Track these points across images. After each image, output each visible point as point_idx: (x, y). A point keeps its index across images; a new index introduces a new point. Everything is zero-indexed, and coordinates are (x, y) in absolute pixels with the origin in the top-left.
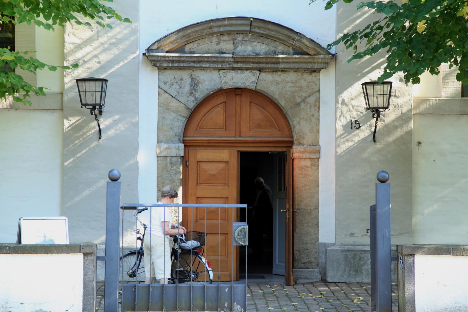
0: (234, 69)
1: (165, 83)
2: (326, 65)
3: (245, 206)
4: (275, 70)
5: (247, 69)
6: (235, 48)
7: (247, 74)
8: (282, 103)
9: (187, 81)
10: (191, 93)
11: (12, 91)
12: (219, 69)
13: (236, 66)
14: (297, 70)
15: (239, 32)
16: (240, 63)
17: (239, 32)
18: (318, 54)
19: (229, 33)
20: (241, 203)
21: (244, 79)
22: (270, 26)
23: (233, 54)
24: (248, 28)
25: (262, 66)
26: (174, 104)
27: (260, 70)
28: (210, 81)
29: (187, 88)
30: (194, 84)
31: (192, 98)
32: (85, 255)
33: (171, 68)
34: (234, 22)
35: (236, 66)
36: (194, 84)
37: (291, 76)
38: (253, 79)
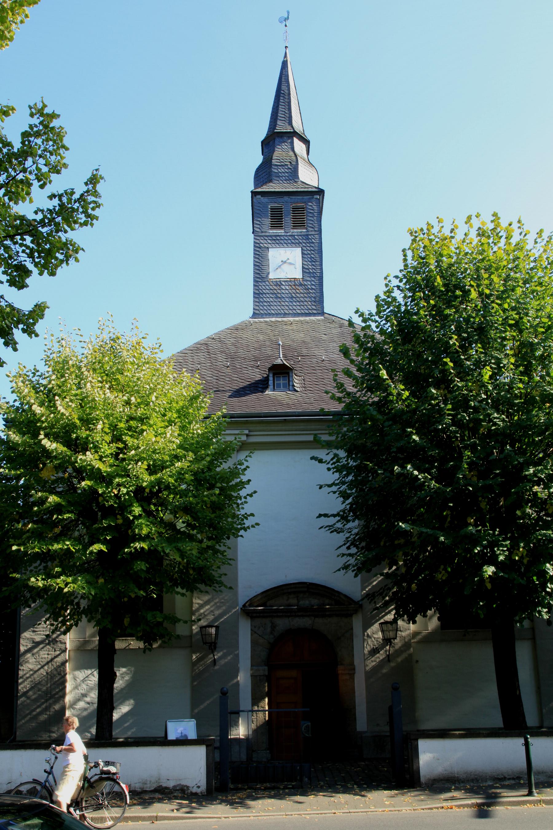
1: (255, 627)
2: (356, 612)
16: (304, 612)
28: (282, 624)
29: (269, 630)
30: (273, 627)
36: (273, 627)
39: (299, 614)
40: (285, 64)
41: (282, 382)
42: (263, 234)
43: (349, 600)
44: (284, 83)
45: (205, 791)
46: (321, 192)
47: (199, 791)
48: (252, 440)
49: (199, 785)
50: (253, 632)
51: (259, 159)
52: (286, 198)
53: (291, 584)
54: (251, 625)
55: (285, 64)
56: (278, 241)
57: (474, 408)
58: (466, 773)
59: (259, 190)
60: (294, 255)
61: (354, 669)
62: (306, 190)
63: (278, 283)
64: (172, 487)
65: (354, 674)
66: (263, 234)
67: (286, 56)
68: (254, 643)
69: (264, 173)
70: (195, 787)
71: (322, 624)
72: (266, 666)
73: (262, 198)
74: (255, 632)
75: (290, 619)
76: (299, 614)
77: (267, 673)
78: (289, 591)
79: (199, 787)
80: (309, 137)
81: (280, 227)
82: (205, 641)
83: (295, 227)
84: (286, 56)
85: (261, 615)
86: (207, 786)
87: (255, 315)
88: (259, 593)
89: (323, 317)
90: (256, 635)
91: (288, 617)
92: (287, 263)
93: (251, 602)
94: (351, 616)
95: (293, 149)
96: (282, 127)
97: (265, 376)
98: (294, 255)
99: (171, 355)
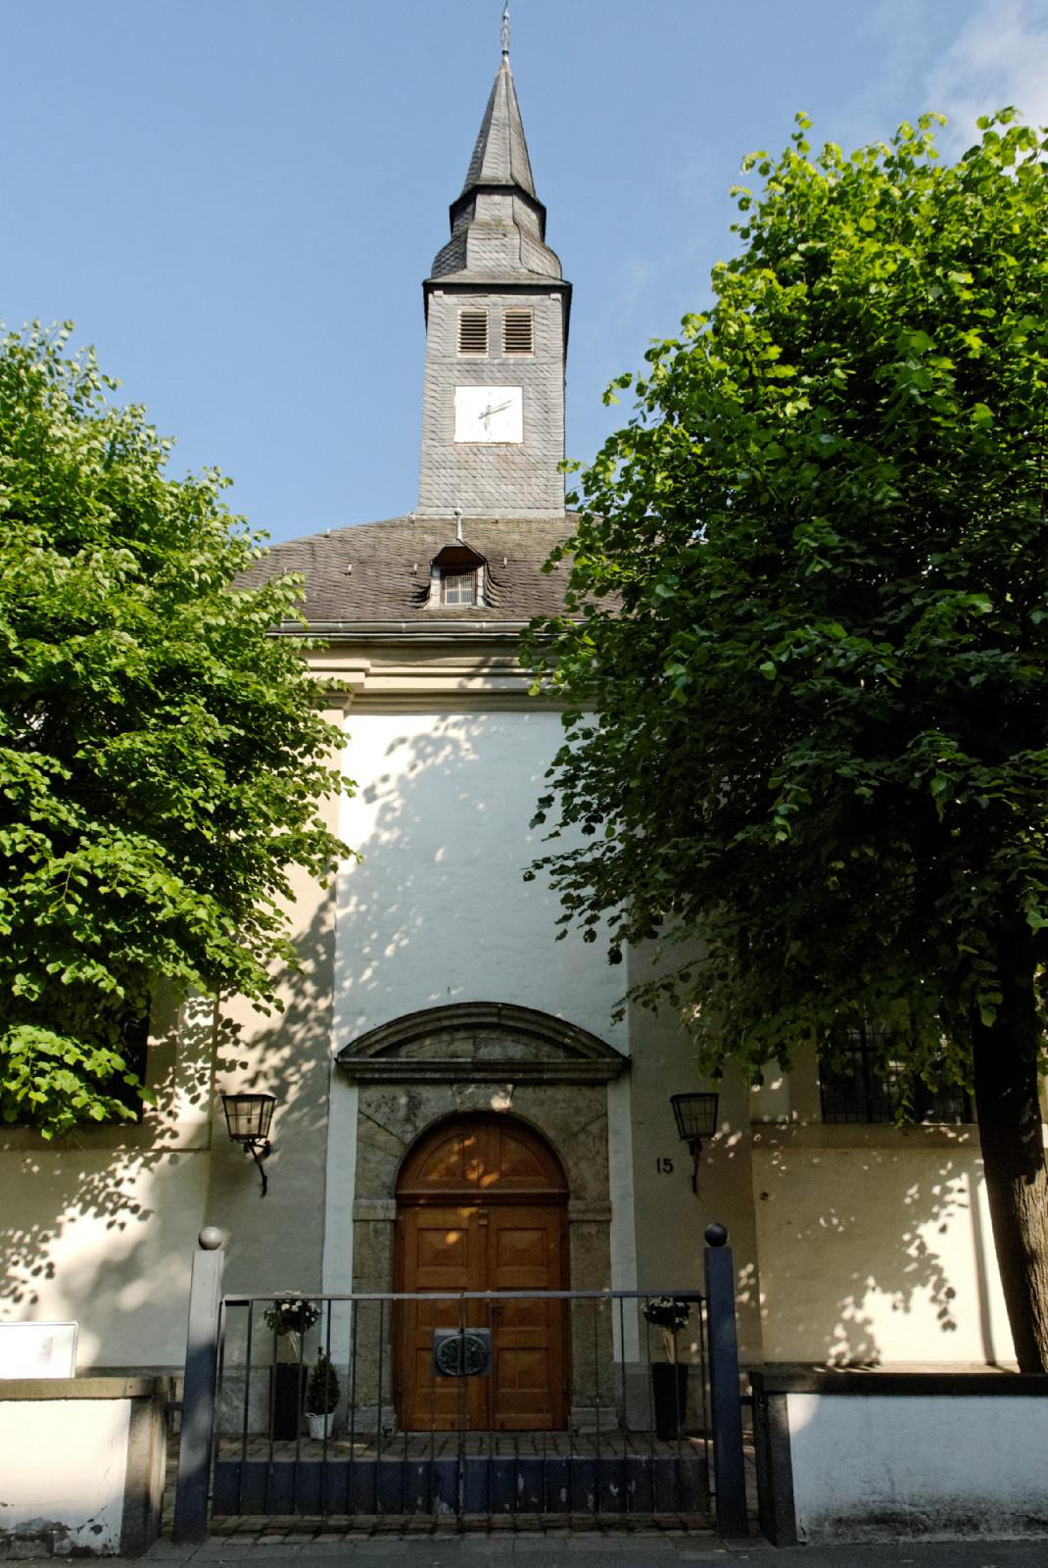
1: (369, 1105)
6: (477, 1049)
8: (551, 1134)
10: (407, 1120)
26: (382, 1137)
28: (438, 1101)
36: (414, 1105)
39: (478, 1076)
42: (448, 360)
43: (603, 1049)
45: (116, 1542)
47: (96, 1542)
49: (99, 1522)
50: (364, 1117)
51: (445, 237)
54: (360, 1101)
57: (932, 273)
58: (932, 1502)
61: (609, 1210)
65: (609, 1221)
66: (448, 360)
68: (365, 1142)
70: (86, 1531)
73: (445, 297)
74: (369, 1118)
75: (455, 1088)
76: (478, 1076)
77: (392, 1215)
78: (455, 1022)
79: (97, 1529)
80: (541, 197)
81: (481, 348)
82: (233, 1132)
83: (509, 349)
85: (385, 1076)
86: (124, 1527)
90: (371, 1124)
91: (450, 1082)
93: (358, 1046)
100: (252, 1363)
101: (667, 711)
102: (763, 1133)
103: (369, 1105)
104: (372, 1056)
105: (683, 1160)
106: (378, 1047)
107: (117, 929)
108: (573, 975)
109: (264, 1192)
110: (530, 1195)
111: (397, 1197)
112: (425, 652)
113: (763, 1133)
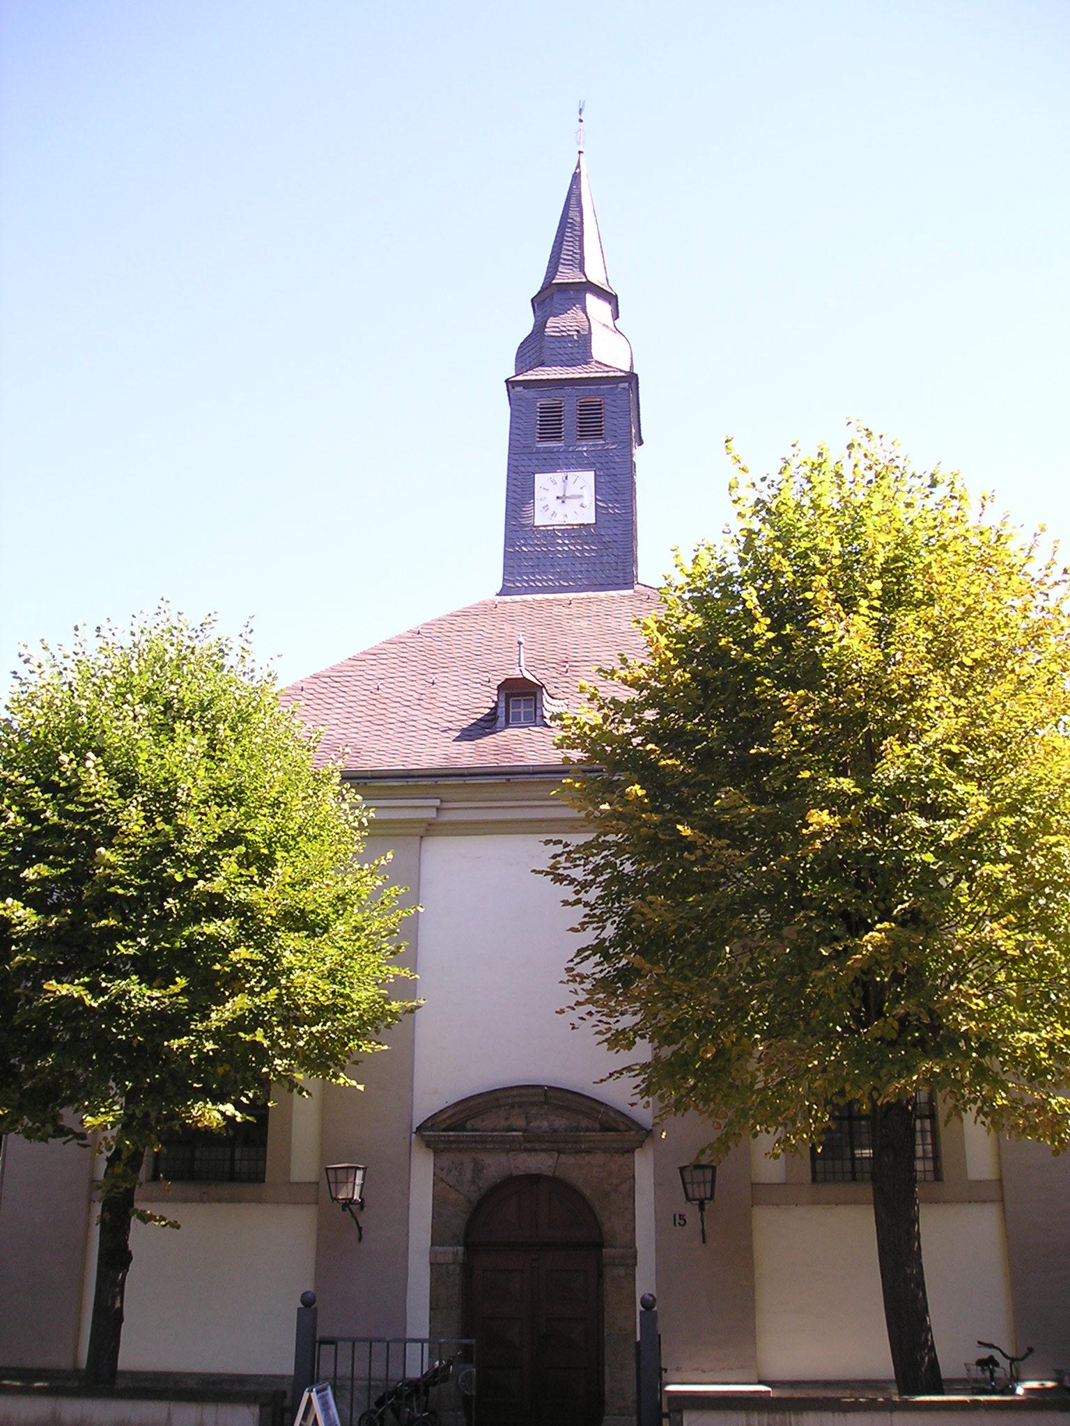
0: (526, 1150)
1: (442, 1169)
2: (641, 1144)
3: (473, 1341)
4: (579, 1152)
5: (542, 1150)
6: (528, 1123)
7: (543, 1156)
8: (588, 1193)
9: (469, 1168)
10: (473, 1182)
11: (658, 910)
12: (508, 1151)
13: (528, 1146)
14: (605, 1151)
15: (533, 1104)
16: (533, 1142)
17: (533, 1104)
18: (631, 1129)
19: (521, 1105)
20: (467, 1337)
21: (538, 1162)
22: (569, 1095)
23: (525, 1131)
24: (542, 1099)
25: (561, 1146)
26: (453, 1196)
27: (560, 1152)
28: (497, 1165)
29: (469, 1176)
30: (478, 1169)
31: (473, 1188)
32: (262, 1406)
33: (449, 1150)
34: (524, 1091)
35: (528, 1146)
36: (478, 1169)
37: (599, 1158)
38: (550, 1162)
40: (576, 178)
41: (522, 710)
43: (632, 1124)
44: (573, 208)
46: (631, 379)
48: (448, 816)
52: (568, 390)
53: (512, 1088)
55: (576, 178)
56: (551, 463)
59: (530, 376)
60: (583, 483)
62: (605, 375)
63: (550, 534)
64: (1061, 881)
67: (578, 166)
69: (533, 350)
71: (580, 1170)
72: (458, 1244)
80: (616, 288)
81: (557, 438)
84: (578, 166)
87: (504, 592)
88: (450, 1103)
89: (631, 592)
92: (566, 499)
94: (631, 1151)
95: (584, 310)
96: (566, 276)
97: (493, 705)
98: (583, 483)
99: (920, 463)
100: (356, 1375)
101: (351, 818)
102: (760, 1193)
103: (442, 1169)
104: (444, 1130)
105: (691, 1211)
106: (449, 1122)
107: (242, 1034)
108: (585, 1056)
109: (360, 1239)
110: (828, 1399)
111: (466, 1245)
112: (433, 772)
113: (760, 1193)
